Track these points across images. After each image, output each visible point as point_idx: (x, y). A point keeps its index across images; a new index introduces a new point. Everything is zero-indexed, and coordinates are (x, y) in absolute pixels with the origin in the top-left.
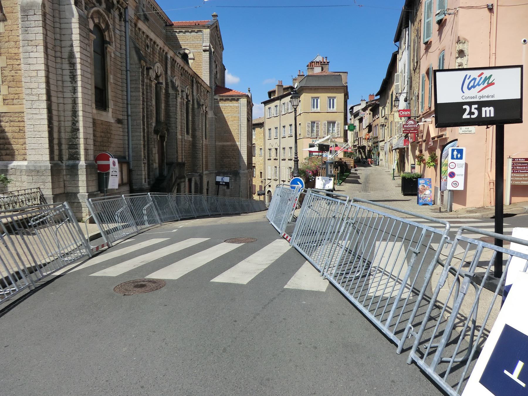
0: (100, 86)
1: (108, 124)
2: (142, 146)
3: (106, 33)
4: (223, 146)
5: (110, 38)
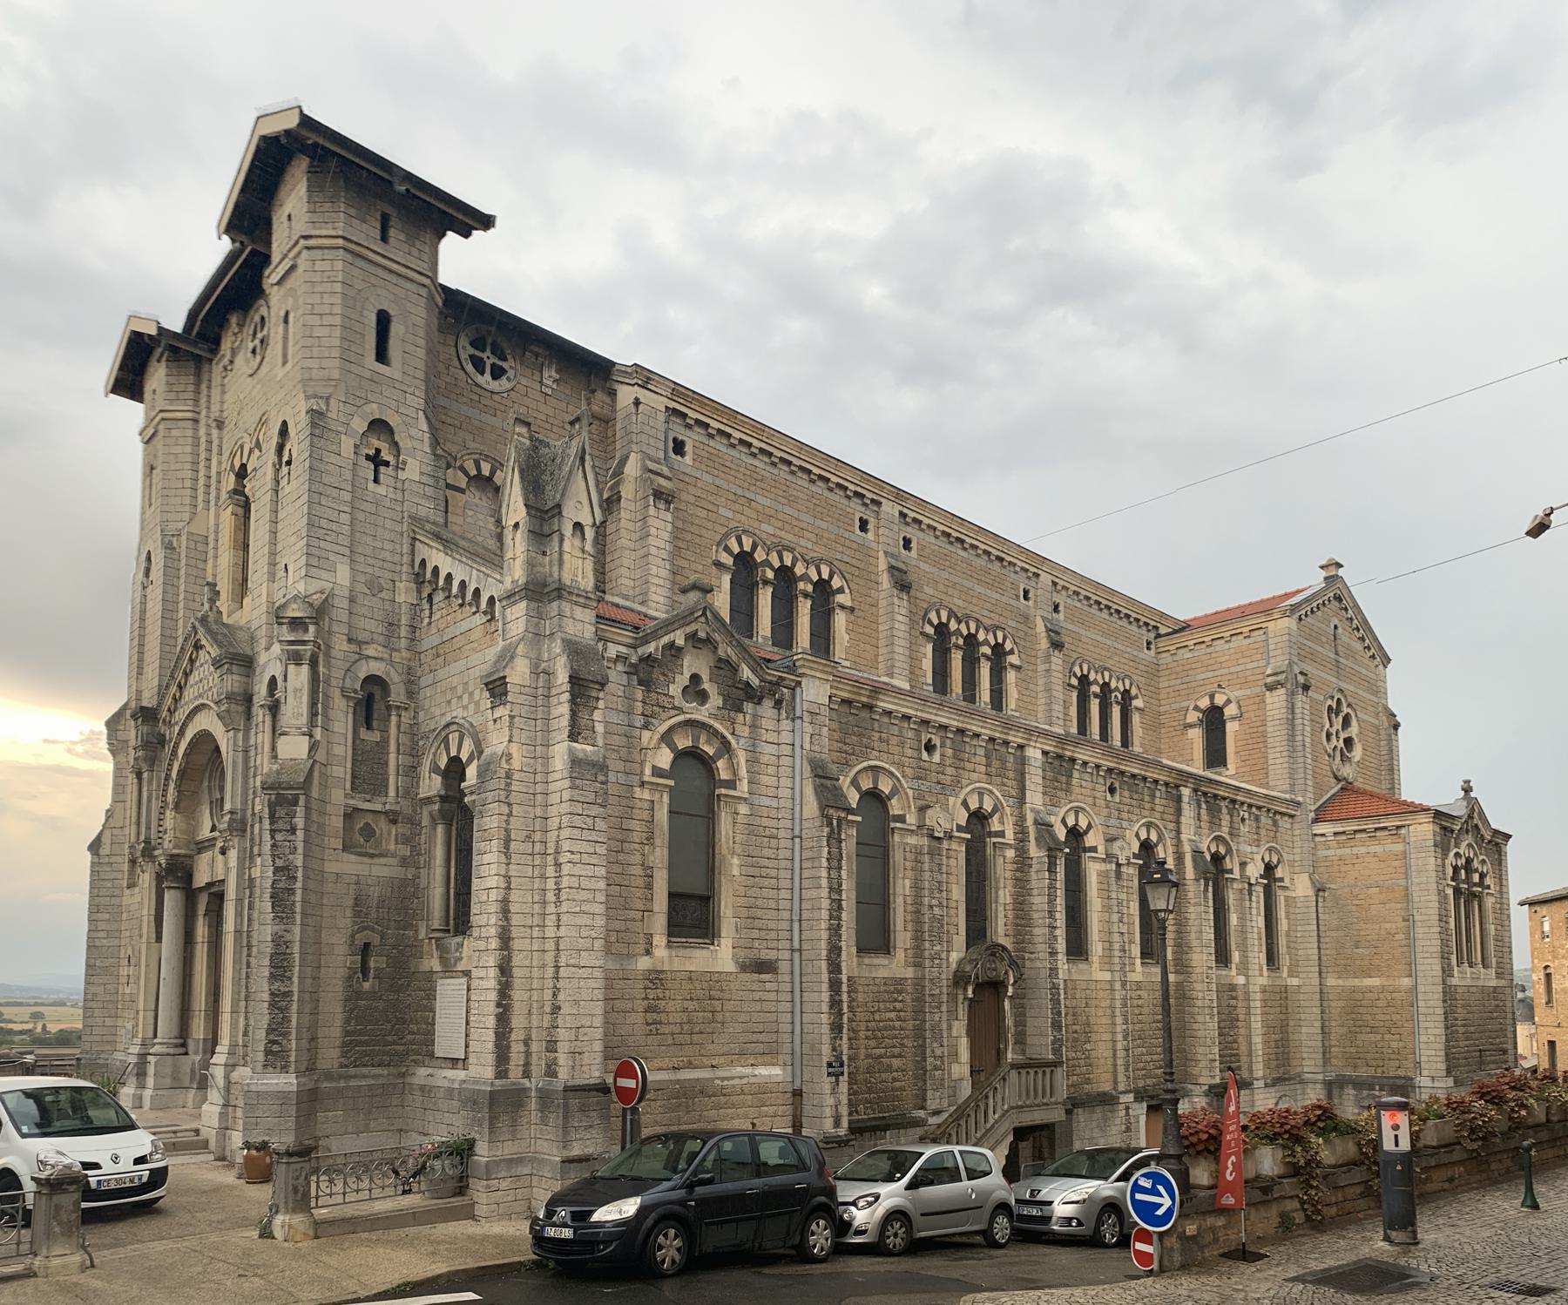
0: (696, 886)
1: (714, 980)
2: (826, 1029)
3: (721, 764)
4: (1354, 990)
5: (734, 771)
